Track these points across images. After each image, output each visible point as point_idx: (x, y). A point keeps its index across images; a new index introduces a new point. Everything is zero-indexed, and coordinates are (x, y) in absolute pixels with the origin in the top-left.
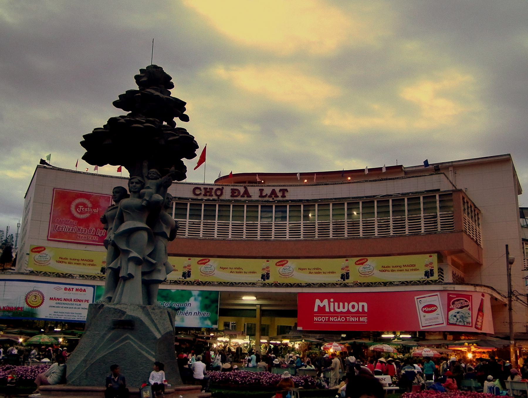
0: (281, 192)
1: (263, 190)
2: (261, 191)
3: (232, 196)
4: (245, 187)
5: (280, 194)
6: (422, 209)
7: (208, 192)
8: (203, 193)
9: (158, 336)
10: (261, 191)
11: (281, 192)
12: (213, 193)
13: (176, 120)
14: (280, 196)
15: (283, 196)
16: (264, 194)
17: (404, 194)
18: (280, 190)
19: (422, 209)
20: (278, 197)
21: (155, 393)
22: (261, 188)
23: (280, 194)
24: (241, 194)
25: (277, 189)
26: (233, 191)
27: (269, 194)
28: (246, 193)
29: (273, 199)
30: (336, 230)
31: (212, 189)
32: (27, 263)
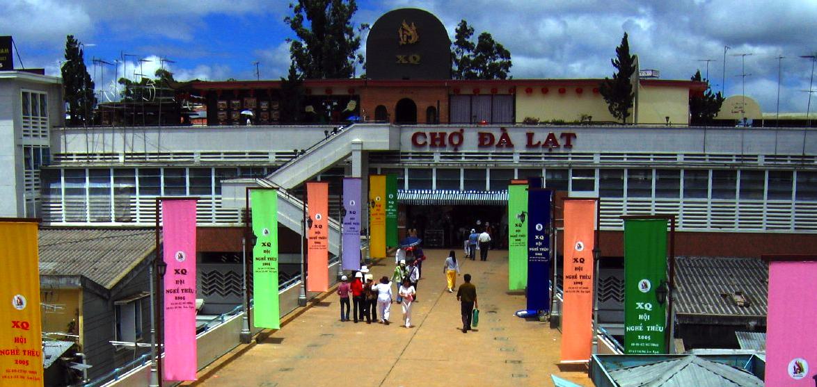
0: (565, 138)
1: (533, 134)
2: (530, 136)
3: (481, 145)
4: (503, 129)
5: (562, 142)
6: (738, 191)
7: (437, 139)
8: (429, 140)
9: (815, 232)
10: (530, 136)
11: (565, 138)
12: (447, 141)
13: (346, 25)
14: (562, 147)
15: (568, 145)
16: (535, 142)
17: (18, 146)
18: (563, 135)
19: (738, 191)
20: (558, 146)
21: (633, 344)
22: (326, 129)
23: (562, 142)
24: (497, 142)
25: (557, 135)
26: (482, 137)
27: (542, 143)
28: (505, 136)
29: (550, 150)
30: (119, 205)
31: (445, 134)
32: (347, 218)
